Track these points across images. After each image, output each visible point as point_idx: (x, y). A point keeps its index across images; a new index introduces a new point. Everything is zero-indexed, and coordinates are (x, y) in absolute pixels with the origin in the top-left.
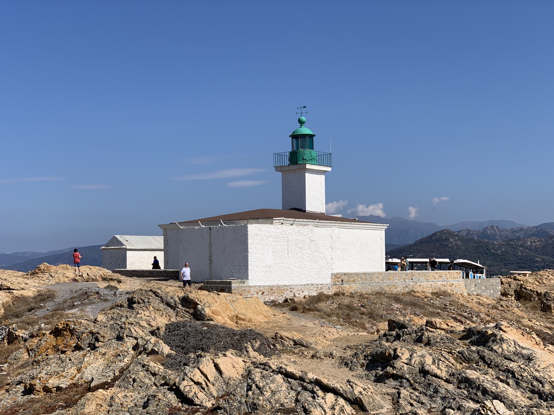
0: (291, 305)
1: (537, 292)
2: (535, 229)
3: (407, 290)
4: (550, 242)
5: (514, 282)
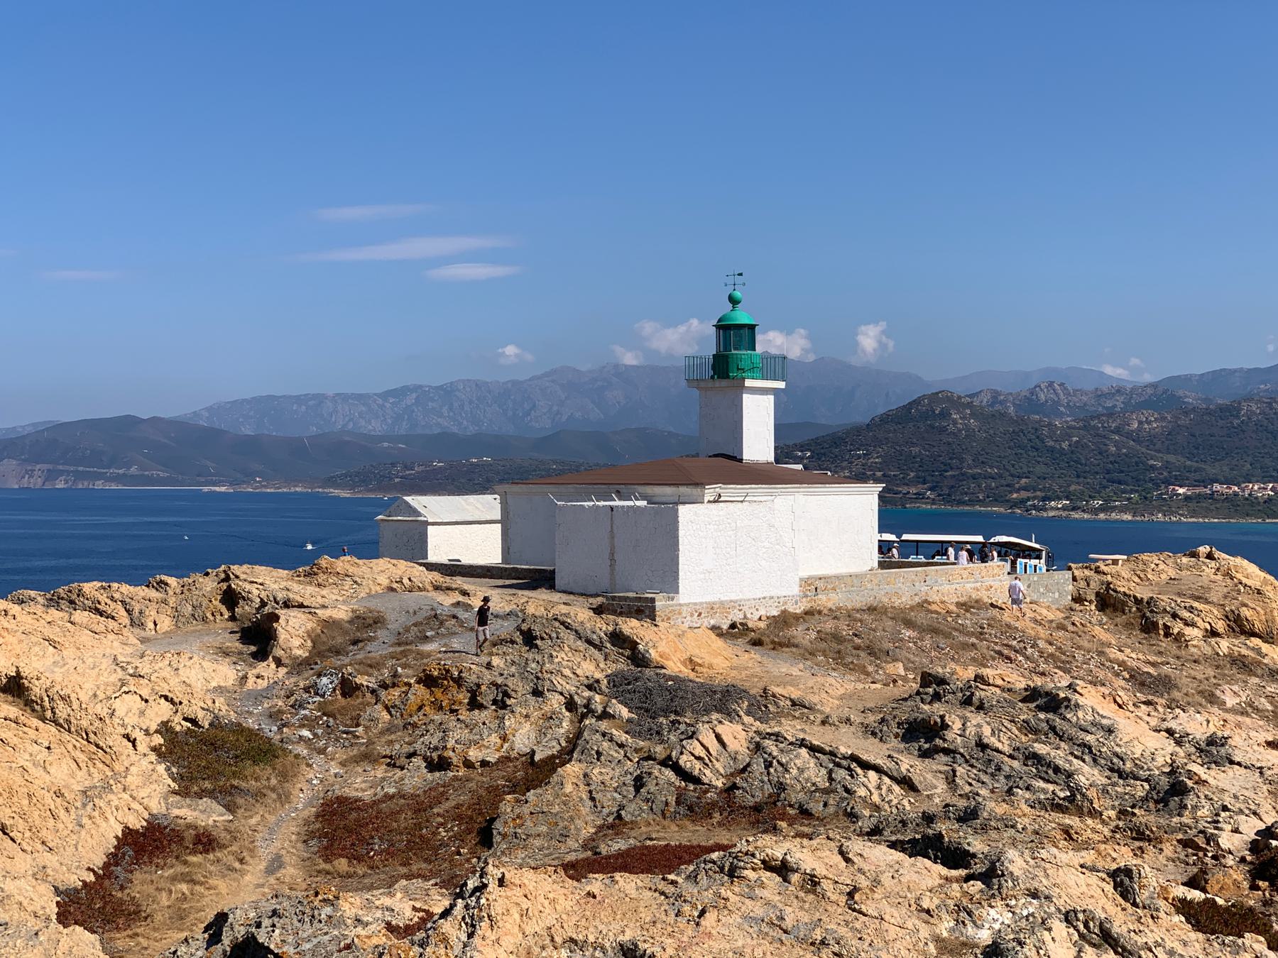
0: (736, 631)
1: (1135, 597)
2: (1150, 391)
3: (917, 599)
5: (1097, 577)
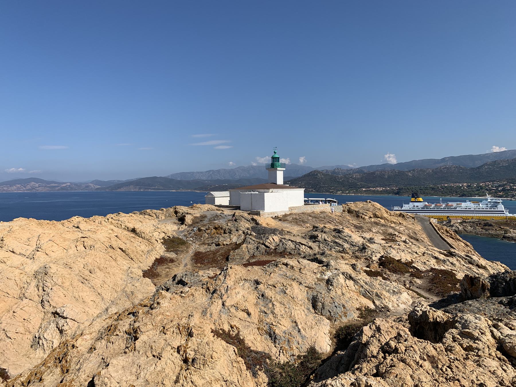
0: (276, 218)
4: (364, 175)
